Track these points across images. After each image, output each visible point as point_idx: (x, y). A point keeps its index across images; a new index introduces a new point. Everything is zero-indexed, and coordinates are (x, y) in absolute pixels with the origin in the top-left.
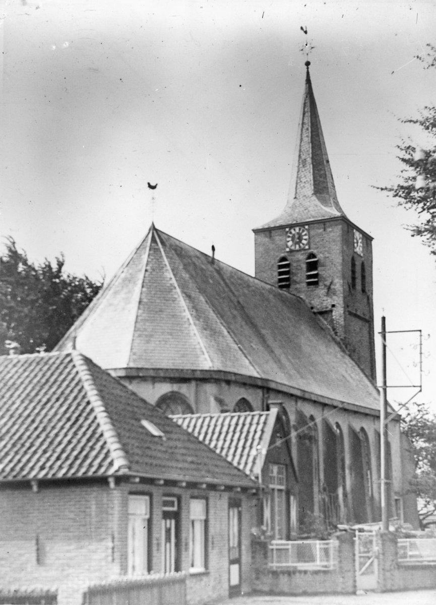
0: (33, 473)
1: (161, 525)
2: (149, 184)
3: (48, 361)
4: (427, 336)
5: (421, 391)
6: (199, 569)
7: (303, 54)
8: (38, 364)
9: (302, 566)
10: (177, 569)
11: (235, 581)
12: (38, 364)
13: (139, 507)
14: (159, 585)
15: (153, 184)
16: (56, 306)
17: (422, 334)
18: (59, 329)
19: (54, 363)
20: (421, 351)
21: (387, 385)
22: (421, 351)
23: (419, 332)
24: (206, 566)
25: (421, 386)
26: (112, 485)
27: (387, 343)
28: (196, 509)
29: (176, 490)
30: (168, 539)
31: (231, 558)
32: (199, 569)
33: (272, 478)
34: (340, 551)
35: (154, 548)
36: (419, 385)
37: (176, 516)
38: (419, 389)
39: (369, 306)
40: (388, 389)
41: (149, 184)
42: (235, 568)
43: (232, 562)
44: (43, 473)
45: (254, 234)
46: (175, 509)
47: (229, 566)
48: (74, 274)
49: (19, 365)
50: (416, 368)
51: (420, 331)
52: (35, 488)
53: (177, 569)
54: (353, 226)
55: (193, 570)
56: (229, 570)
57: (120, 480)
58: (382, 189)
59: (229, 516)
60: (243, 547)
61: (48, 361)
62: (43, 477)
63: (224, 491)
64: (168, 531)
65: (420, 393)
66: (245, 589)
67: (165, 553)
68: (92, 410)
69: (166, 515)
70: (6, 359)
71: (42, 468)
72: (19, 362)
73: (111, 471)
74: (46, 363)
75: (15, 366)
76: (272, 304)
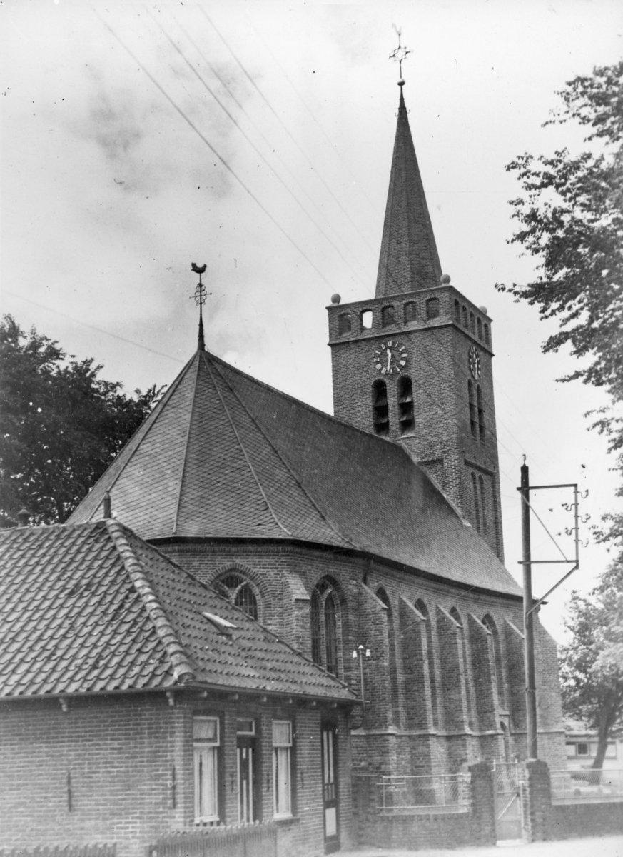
1: (237, 755)
3: (71, 533)
4: (584, 494)
5: (577, 567)
6: (284, 814)
7: (405, 48)
8: (58, 537)
9: (420, 810)
10: (257, 815)
11: (331, 829)
12: (58, 537)
13: (206, 728)
14: (233, 839)
15: (200, 265)
17: (579, 490)
18: (593, 681)
24: (294, 809)
25: (577, 561)
27: (531, 503)
28: (279, 734)
29: (253, 707)
31: (326, 798)
32: (284, 814)
33: (191, 776)
34: (473, 789)
36: (574, 559)
37: (253, 744)
38: (574, 565)
40: (533, 566)
41: (194, 265)
42: (331, 813)
43: (328, 804)
44: (115, 683)
45: (327, 311)
47: (324, 810)
49: (32, 539)
51: (575, 486)
54: (490, 517)
55: (278, 816)
56: (324, 816)
59: (322, 739)
60: (342, 785)
63: (316, 708)
64: (244, 764)
65: (576, 571)
68: (138, 599)
69: (242, 742)
71: (72, 679)
72: (32, 534)
73: (167, 684)
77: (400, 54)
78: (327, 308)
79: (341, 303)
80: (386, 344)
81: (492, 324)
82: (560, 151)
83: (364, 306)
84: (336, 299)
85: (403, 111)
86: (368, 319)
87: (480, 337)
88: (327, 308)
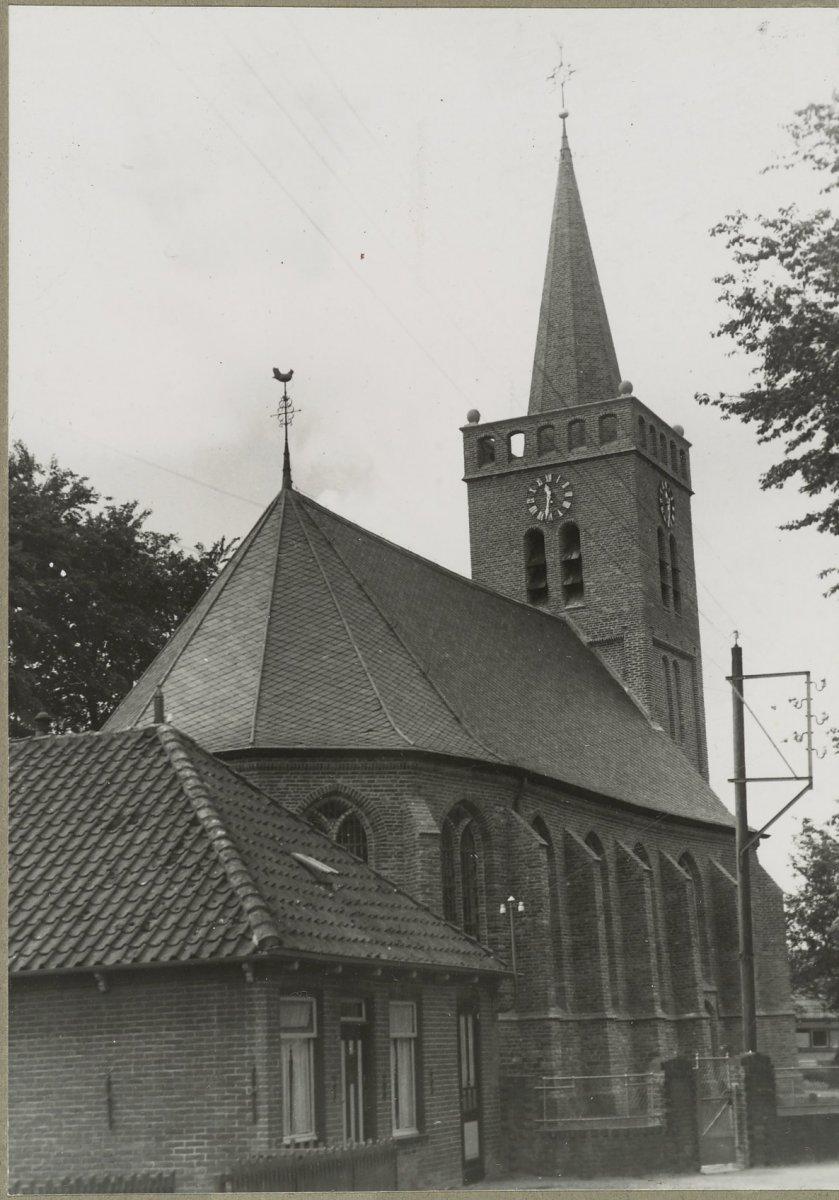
0: (97, 956)
2: (276, 371)
3: (109, 744)
4: (821, 684)
5: (810, 786)
10: (370, 1132)
11: (472, 1149)
12: (90, 750)
13: (298, 1013)
16: (40, 661)
17: (812, 679)
19: (121, 748)
20: (809, 712)
21: (748, 776)
22: (809, 712)
23: (805, 676)
24: (420, 1120)
25: (810, 778)
26: (249, 977)
28: (400, 1023)
30: (351, 1079)
35: (330, 1094)
36: (807, 775)
37: (365, 1034)
38: (806, 783)
39: (699, 747)
41: (276, 371)
42: (471, 1128)
43: (467, 1116)
46: (363, 1019)
48: (199, 547)
50: (802, 743)
52: (102, 986)
53: (370, 1132)
57: (261, 966)
58: (767, 169)
61: (109, 744)
62: (114, 964)
64: (351, 1061)
65: (809, 792)
66: (491, 1163)
67: (347, 1105)
69: (348, 1032)
70: (31, 742)
71: (111, 947)
74: (105, 749)
75: (46, 754)
76: (336, 887)
77: (562, 75)
78: (461, 429)
79: (481, 422)
80: (543, 479)
81: (690, 449)
82: (786, 208)
83: (513, 426)
84: (474, 416)
85: (566, 153)
86: (518, 445)
87: (674, 468)
88: (461, 429)
